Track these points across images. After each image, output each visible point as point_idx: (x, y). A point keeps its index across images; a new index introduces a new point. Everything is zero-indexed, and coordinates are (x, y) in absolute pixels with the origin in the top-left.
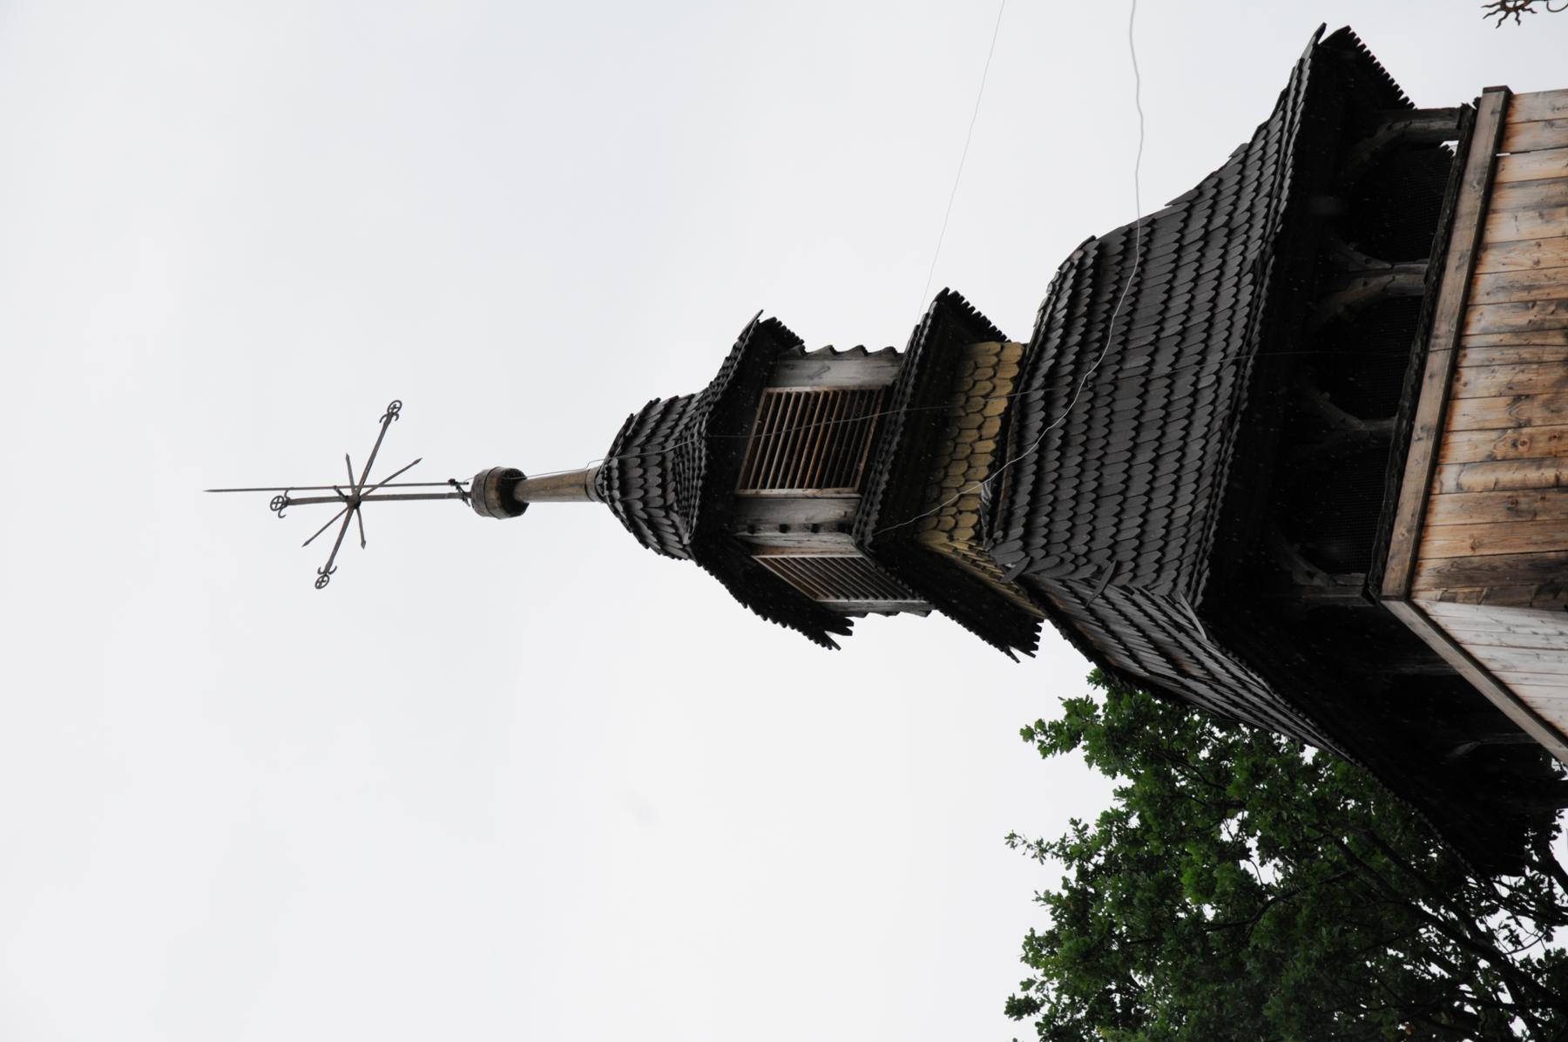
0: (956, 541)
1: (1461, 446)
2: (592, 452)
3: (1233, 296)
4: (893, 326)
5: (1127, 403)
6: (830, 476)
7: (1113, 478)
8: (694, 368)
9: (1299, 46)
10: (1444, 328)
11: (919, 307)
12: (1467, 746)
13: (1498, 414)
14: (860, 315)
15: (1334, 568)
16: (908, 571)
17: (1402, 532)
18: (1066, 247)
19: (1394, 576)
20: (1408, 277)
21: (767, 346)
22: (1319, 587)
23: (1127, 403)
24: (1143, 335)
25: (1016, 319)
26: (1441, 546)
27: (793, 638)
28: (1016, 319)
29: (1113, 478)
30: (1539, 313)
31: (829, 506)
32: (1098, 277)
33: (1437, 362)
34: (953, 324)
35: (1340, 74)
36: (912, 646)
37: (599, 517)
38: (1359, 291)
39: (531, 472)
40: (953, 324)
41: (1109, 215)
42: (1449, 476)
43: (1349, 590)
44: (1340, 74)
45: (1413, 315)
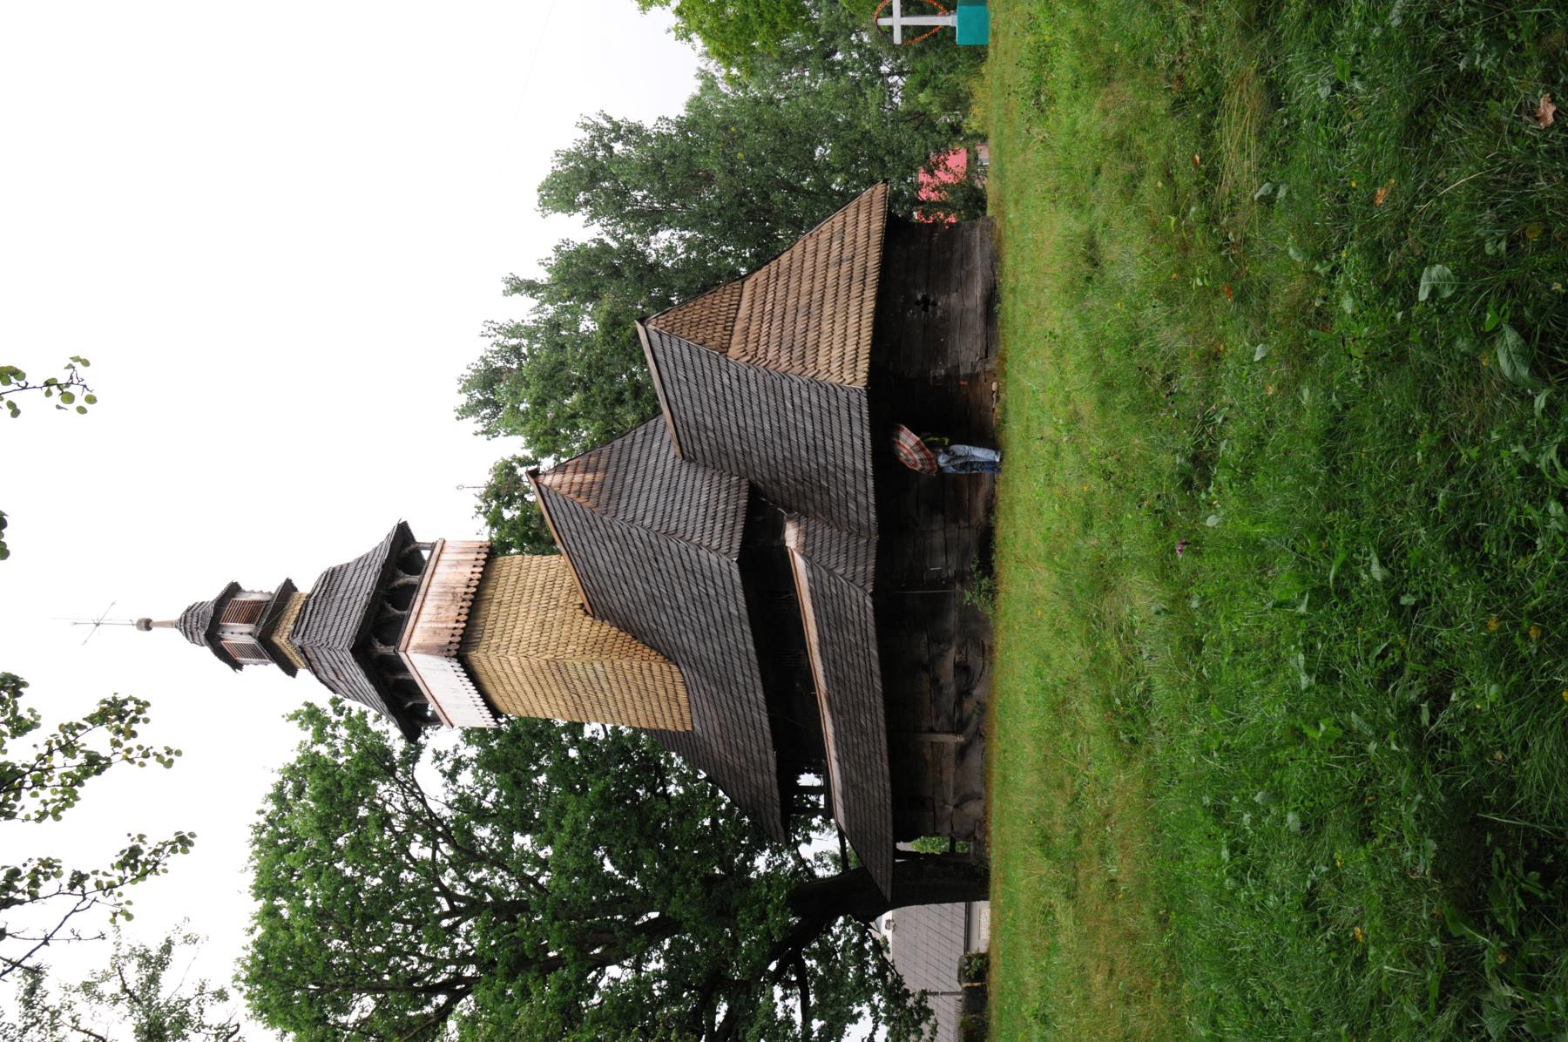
0: (280, 639)
1: (423, 618)
2: (176, 615)
3: (369, 581)
4: (272, 586)
5: (336, 605)
6: (248, 621)
7: (330, 622)
8: (211, 594)
9: (395, 524)
10: (422, 591)
11: (280, 582)
12: (720, 1018)
13: (434, 611)
14: (260, 584)
15: (386, 644)
16: (268, 650)
17: (406, 637)
18: (325, 569)
19: (402, 647)
20: (414, 579)
21: (234, 589)
22: (382, 649)
23: (336, 605)
24: (343, 588)
25: (305, 586)
26: (415, 641)
27: (227, 667)
28: (305, 586)
29: (330, 622)
30: (399, 577)
31: (248, 628)
32: (331, 578)
33: (420, 598)
34: (288, 588)
35: (403, 534)
36: (266, 673)
37: (177, 635)
38: (401, 581)
39: (155, 620)
40: (288, 588)
41: (336, 563)
42: (419, 625)
43: (389, 650)
44: (403, 534)
45: (414, 588)
